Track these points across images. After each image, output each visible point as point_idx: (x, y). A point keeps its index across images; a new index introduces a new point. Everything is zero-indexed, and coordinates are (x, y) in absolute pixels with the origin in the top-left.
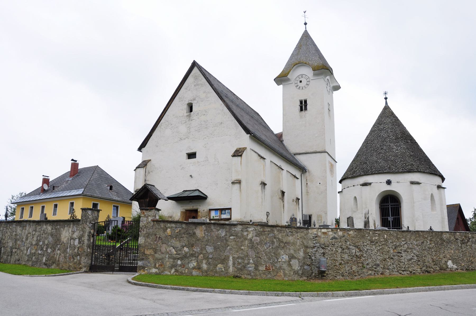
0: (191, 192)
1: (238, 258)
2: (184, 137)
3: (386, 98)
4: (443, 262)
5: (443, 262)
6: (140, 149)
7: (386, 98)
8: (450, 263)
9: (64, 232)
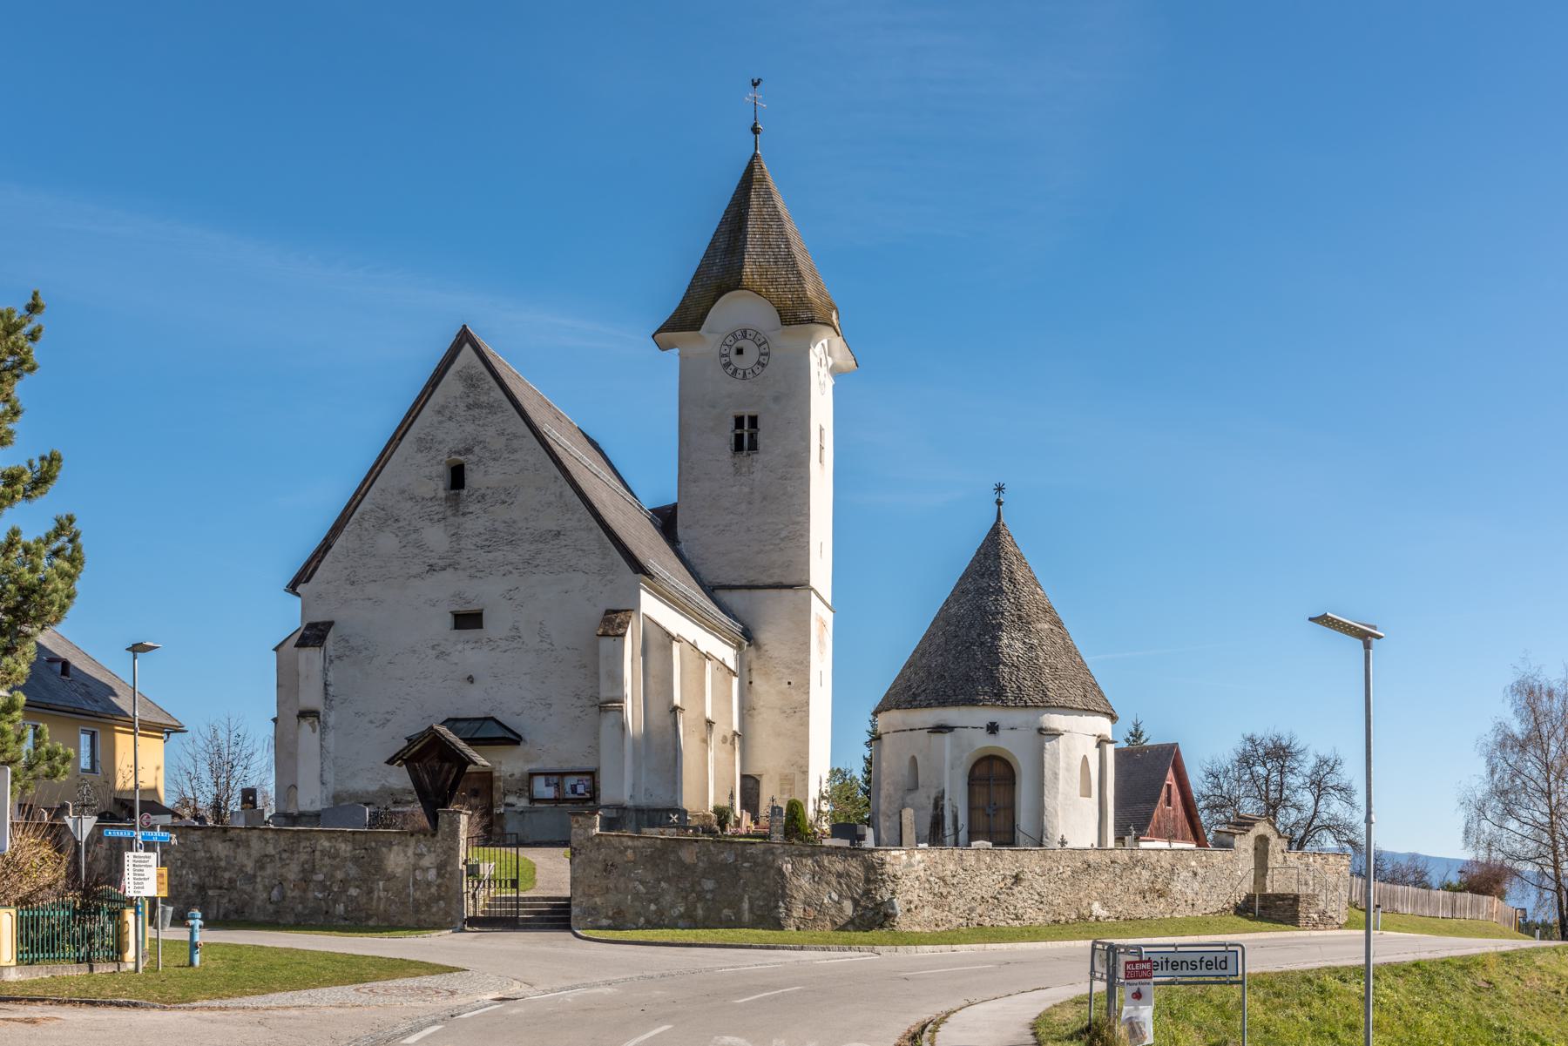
0: (477, 724)
2: (441, 563)
4: (1085, 904)
5: (1085, 904)
6: (293, 587)
7: (999, 503)
8: (1097, 908)
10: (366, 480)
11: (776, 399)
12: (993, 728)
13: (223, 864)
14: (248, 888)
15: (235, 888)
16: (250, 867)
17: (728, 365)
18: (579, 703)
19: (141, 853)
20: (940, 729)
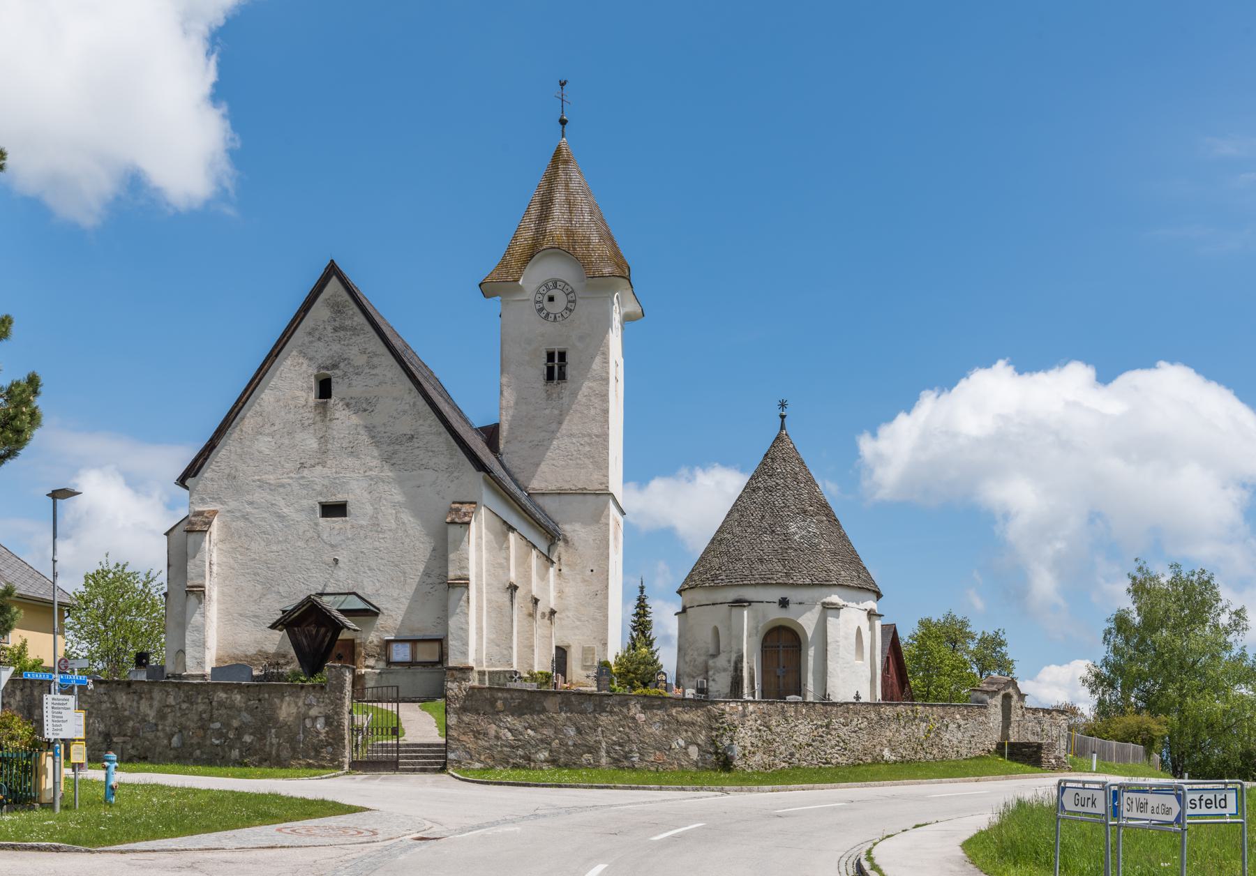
1: (615, 743)
2: (312, 462)
3: (783, 417)
6: (182, 481)
7: (783, 417)
9: (284, 706)
10: (246, 390)
11: (581, 338)
12: (784, 603)
13: (127, 713)
14: (150, 736)
15: (137, 736)
16: (152, 715)
17: (542, 309)
18: (430, 581)
19: (59, 696)
20: (739, 603)
